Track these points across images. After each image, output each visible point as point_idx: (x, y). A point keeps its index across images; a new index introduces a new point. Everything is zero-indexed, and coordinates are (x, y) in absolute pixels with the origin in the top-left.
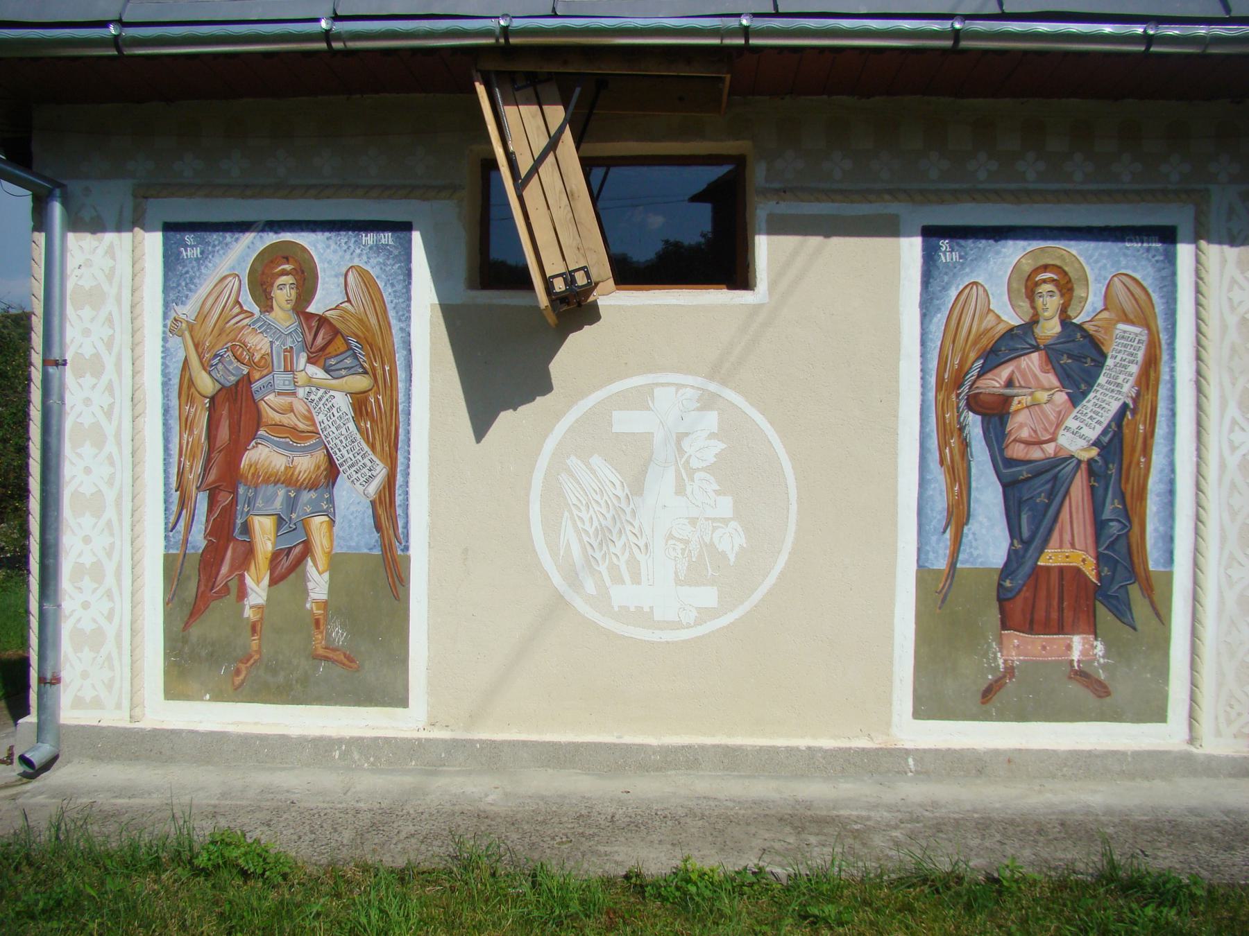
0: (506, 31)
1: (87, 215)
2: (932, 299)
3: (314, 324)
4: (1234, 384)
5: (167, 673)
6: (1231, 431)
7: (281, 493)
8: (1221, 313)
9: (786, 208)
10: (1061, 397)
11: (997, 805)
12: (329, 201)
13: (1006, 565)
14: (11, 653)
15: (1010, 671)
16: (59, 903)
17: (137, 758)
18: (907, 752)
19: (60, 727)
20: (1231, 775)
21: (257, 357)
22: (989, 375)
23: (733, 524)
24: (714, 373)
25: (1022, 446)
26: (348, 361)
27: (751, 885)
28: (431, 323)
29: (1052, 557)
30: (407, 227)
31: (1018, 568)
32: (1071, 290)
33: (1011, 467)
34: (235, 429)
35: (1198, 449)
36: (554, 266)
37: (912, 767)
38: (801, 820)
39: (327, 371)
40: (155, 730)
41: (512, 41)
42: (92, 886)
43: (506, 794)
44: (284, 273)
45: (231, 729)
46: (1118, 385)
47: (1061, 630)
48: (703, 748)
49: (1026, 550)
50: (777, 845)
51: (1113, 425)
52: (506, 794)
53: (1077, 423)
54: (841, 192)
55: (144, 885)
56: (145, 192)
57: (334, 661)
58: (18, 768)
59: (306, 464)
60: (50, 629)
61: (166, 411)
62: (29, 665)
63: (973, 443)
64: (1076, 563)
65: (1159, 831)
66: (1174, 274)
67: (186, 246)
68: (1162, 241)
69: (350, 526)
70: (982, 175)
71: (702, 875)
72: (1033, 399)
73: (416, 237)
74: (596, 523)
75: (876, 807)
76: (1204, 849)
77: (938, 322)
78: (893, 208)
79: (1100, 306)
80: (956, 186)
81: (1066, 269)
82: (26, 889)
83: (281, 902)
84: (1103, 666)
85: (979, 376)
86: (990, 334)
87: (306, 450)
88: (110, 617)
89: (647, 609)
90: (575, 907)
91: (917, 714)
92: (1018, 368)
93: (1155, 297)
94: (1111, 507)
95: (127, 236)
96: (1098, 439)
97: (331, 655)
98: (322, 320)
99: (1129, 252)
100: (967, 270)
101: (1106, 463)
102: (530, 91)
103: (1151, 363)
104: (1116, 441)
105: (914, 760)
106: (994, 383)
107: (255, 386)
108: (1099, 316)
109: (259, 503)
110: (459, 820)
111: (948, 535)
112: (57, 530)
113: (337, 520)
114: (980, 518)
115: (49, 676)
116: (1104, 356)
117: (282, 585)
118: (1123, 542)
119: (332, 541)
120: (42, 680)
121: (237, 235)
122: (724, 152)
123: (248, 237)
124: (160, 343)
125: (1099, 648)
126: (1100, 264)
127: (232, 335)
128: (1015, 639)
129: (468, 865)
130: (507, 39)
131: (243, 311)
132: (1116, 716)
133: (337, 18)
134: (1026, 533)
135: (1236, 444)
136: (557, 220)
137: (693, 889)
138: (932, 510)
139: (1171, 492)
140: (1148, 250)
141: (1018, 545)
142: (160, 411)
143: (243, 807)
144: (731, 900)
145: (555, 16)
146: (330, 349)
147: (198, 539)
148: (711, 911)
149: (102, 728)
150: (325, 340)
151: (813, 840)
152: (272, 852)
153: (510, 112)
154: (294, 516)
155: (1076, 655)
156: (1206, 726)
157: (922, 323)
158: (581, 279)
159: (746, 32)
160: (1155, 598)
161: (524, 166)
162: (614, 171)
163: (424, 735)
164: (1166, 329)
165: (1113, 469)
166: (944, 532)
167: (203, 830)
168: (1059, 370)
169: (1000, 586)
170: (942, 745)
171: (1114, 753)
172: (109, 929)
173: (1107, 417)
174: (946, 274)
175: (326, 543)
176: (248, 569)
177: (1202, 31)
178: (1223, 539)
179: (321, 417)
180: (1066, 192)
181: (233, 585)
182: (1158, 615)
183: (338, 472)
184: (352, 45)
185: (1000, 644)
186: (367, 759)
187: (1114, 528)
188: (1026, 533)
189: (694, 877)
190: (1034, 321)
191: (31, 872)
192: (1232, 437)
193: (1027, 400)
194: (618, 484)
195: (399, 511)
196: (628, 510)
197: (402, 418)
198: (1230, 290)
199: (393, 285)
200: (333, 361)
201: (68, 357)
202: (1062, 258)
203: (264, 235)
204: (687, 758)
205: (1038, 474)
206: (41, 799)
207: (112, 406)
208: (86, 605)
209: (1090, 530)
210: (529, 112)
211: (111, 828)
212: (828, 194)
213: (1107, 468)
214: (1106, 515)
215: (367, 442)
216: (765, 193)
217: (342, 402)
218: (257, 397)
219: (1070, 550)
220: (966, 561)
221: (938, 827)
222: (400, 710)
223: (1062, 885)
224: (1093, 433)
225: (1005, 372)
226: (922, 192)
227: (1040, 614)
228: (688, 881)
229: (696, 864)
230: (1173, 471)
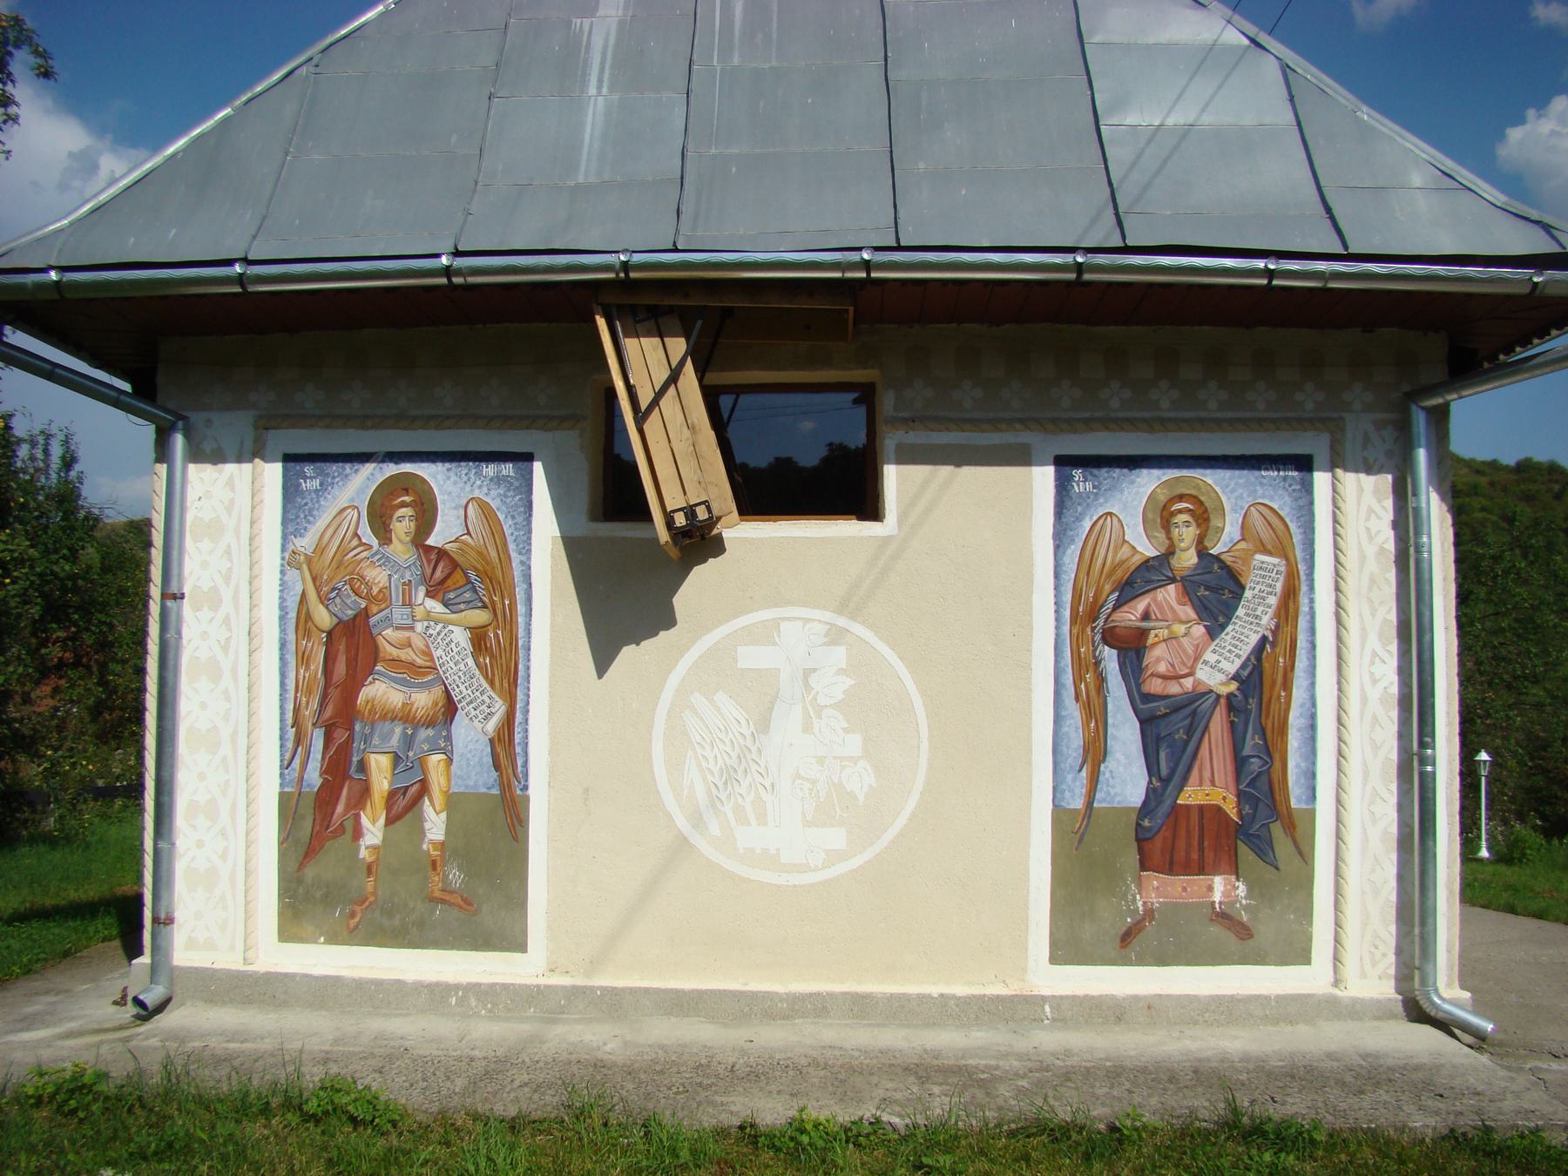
0: (626, 266)
1: (208, 446)
3: (433, 557)
5: (280, 914)
6: (1372, 663)
7: (398, 730)
9: (915, 437)
10: (1199, 630)
11: (1132, 1053)
12: (451, 432)
13: (1144, 803)
14: (127, 889)
15: (1149, 913)
16: (170, 1145)
17: (250, 1002)
18: (1044, 999)
19: (173, 969)
20: (1377, 1018)
21: (375, 591)
22: (1125, 608)
23: (862, 763)
24: (842, 608)
25: (1160, 681)
26: (467, 595)
27: (868, 1135)
28: (553, 557)
29: (1192, 795)
30: (528, 458)
32: (1207, 520)
34: (352, 664)
35: (1339, 683)
36: (674, 500)
38: (924, 1070)
39: (446, 605)
40: (268, 973)
41: (632, 275)
42: (202, 1129)
43: (625, 1043)
44: (404, 505)
45: (345, 973)
46: (1257, 617)
47: (1202, 870)
48: (831, 995)
49: (1165, 788)
50: (898, 1096)
52: (625, 1043)
55: (255, 1130)
56: (267, 422)
57: (451, 904)
58: (131, 1010)
59: (423, 700)
60: (164, 867)
61: (283, 646)
62: (142, 905)
64: (1216, 800)
65: (1293, 1077)
66: (1311, 503)
67: (305, 478)
68: (1298, 469)
69: (468, 765)
70: (1115, 404)
71: (817, 1125)
73: (538, 467)
74: (720, 762)
75: (1006, 1055)
76: (1333, 1094)
78: (1026, 437)
79: (1237, 537)
80: (1087, 415)
82: (139, 1131)
83: (390, 1150)
84: (1246, 908)
85: (1115, 609)
87: (422, 686)
88: (224, 857)
89: (773, 852)
90: (685, 1155)
91: (1054, 959)
92: (1155, 600)
93: (1292, 527)
94: (1251, 743)
95: (247, 467)
97: (447, 898)
98: (442, 553)
101: (1246, 698)
102: (652, 323)
103: (1290, 595)
104: (1256, 674)
106: (1130, 616)
107: (373, 621)
108: (1238, 546)
109: (376, 741)
110: (575, 1069)
111: (1084, 773)
112: (173, 766)
113: (456, 758)
114: (1118, 755)
115: (163, 916)
116: (1243, 588)
117: (399, 824)
118: (1264, 778)
119: (449, 780)
120: (156, 920)
121: (357, 466)
122: (854, 380)
123: (369, 468)
124: (279, 576)
125: (1242, 889)
127: (350, 569)
128: (1154, 880)
129: (581, 1114)
130: (627, 274)
131: (361, 544)
132: (1259, 959)
133: (457, 254)
134: (1164, 771)
136: (679, 455)
137: (805, 1139)
139: (1313, 727)
140: (1285, 479)
142: (276, 646)
143: (354, 1053)
144: (844, 1150)
145: (676, 250)
146: (449, 582)
147: (314, 777)
148: (824, 1161)
149: (216, 970)
150: (445, 573)
151: (936, 1090)
152: (382, 1098)
153: (630, 344)
154: (411, 754)
155: (1217, 897)
158: (702, 514)
159: (867, 265)
161: (645, 400)
162: (745, 400)
163: (542, 981)
164: (1305, 560)
167: (313, 1075)
169: (1138, 824)
170: (1080, 992)
171: (1257, 997)
172: (219, 1172)
173: (1245, 651)
175: (443, 781)
176: (363, 808)
177: (1321, 266)
178: (1366, 774)
179: (439, 652)
180: (1201, 420)
181: (349, 825)
182: (1301, 854)
183: (456, 709)
184: (472, 280)
185: (1140, 885)
186: (484, 1007)
187: (1255, 765)
188: (1164, 771)
189: (809, 1127)
190: (1170, 552)
191: (144, 1113)
193: (1164, 633)
194: (743, 722)
195: (518, 749)
196: (754, 749)
197: (521, 653)
198: (1368, 519)
199: (513, 517)
200: (452, 595)
201: (186, 590)
202: (1197, 487)
203: (384, 466)
204: (816, 1006)
205: (1176, 709)
206: (154, 1042)
207: (228, 640)
208: (200, 844)
209: (1230, 767)
210: (651, 344)
211: (224, 1071)
212: (961, 423)
213: (1247, 703)
214: (1247, 751)
215: (486, 678)
216: (894, 422)
217: (461, 637)
218: (375, 631)
219: (1210, 787)
220: (1104, 800)
221: (1067, 1076)
222: (518, 955)
223: (1184, 1133)
224: (1232, 667)
225: (1141, 605)
226: (1053, 421)
227: (1180, 855)
228: (803, 1131)
229: (812, 1114)
230: (1314, 705)
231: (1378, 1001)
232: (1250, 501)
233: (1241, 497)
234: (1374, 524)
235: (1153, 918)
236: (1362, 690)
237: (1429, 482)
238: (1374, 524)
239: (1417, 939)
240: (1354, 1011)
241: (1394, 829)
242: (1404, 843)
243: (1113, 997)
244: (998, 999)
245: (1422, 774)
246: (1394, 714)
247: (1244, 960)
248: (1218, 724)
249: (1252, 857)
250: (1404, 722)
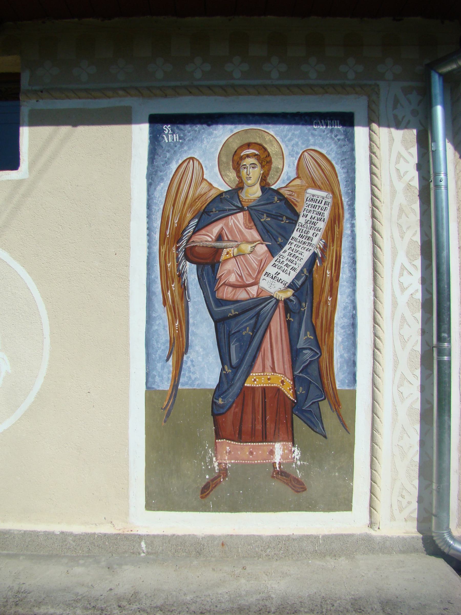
2: (156, 172)
4: (402, 238)
6: (401, 275)
8: (391, 181)
9: (44, 104)
10: (262, 249)
13: (218, 386)
15: (224, 471)
18: (140, 537)
22: (203, 232)
25: (230, 289)
29: (257, 379)
31: (228, 389)
33: (222, 306)
35: (375, 290)
37: (144, 549)
47: (265, 438)
49: (235, 374)
51: (305, 271)
53: (275, 270)
54: (86, 90)
63: (190, 287)
64: (276, 384)
66: (353, 149)
68: (343, 124)
70: (198, 75)
72: (239, 251)
77: (162, 189)
78: (127, 102)
79: (293, 175)
80: (178, 83)
81: (266, 146)
84: (301, 468)
85: (194, 233)
86: (203, 199)
91: (149, 506)
92: (227, 225)
93: (337, 167)
96: (293, 282)
99: (316, 133)
100: (186, 148)
103: (335, 220)
104: (308, 283)
105: (146, 543)
106: (207, 237)
111: (170, 362)
114: (197, 348)
116: (297, 215)
125: (297, 453)
126: (292, 143)
128: (227, 446)
132: (311, 506)
134: (234, 361)
135: (405, 285)
138: (157, 342)
139: (354, 325)
141: (228, 370)
155: (277, 459)
156: (382, 513)
157: (148, 191)
160: (342, 411)
164: (347, 193)
165: (305, 307)
166: (168, 360)
168: (260, 227)
169: (213, 402)
170: (169, 532)
171: (308, 537)
173: (300, 265)
174: (168, 151)
180: (265, 86)
182: (344, 425)
185: (215, 450)
188: (234, 361)
190: (240, 187)
192: (402, 280)
198: (397, 162)
205: (244, 312)
209: (287, 357)
213: (301, 306)
214: (301, 344)
219: (271, 373)
220: (187, 384)
224: (289, 279)
225: (215, 229)
227: (247, 426)
230: (355, 308)
231: (404, 539)
232: (304, 148)
233: (297, 144)
234: (402, 166)
235: (226, 476)
236: (393, 295)
237: (446, 135)
238: (402, 166)
239: (434, 493)
240: (385, 546)
241: (418, 406)
242: (425, 416)
243: (194, 536)
244: (105, 536)
245: (440, 363)
246: (419, 315)
247: (298, 508)
248: (277, 323)
249: (305, 427)
250: (426, 321)
